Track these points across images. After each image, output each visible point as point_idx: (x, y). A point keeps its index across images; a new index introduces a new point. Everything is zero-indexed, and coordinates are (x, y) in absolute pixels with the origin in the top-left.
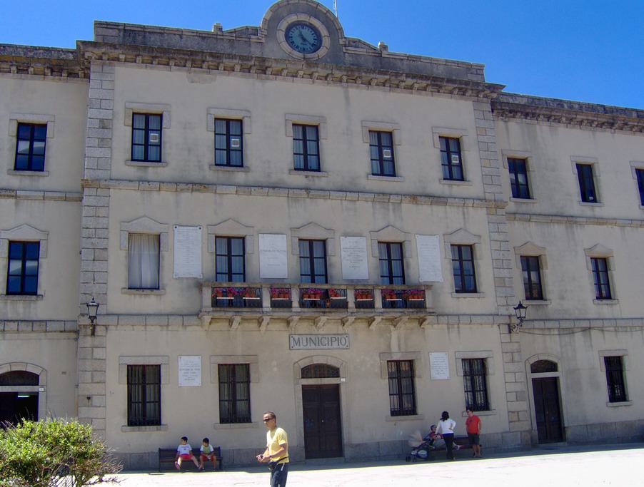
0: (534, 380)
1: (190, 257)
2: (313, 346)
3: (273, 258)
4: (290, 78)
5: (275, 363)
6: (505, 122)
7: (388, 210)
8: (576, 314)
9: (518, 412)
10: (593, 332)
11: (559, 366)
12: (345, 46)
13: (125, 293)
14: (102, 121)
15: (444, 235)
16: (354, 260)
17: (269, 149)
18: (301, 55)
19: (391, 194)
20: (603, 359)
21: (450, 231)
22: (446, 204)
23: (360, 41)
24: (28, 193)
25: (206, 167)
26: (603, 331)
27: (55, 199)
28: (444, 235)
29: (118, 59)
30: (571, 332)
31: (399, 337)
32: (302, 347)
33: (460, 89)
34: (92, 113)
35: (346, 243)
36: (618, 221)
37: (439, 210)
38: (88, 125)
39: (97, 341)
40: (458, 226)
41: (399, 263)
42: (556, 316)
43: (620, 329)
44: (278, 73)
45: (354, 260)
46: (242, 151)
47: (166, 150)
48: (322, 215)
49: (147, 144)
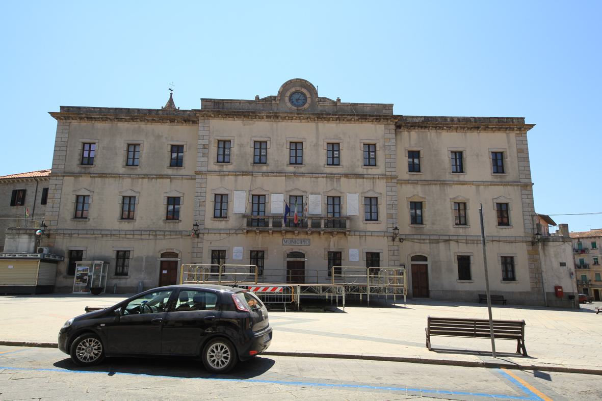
0: (412, 265)
1: (239, 204)
2: (293, 244)
3: (276, 205)
4: (290, 121)
6: (409, 132)
7: (334, 181)
10: (451, 242)
11: (428, 259)
12: (318, 102)
13: (212, 220)
14: (204, 145)
15: (361, 193)
16: (316, 206)
17: (278, 155)
18: (296, 108)
19: (335, 174)
20: (456, 257)
22: (363, 178)
23: (326, 98)
24: (175, 177)
25: (249, 164)
26: (458, 242)
27: (187, 179)
28: (361, 193)
29: (211, 117)
30: (437, 241)
31: (334, 243)
32: (288, 244)
34: (200, 142)
35: (311, 197)
36: (474, 183)
37: (360, 181)
38: (198, 147)
41: (338, 206)
42: (429, 233)
43: (469, 241)
44: (285, 118)
45: (316, 206)
46: (375, 158)
48: (302, 184)
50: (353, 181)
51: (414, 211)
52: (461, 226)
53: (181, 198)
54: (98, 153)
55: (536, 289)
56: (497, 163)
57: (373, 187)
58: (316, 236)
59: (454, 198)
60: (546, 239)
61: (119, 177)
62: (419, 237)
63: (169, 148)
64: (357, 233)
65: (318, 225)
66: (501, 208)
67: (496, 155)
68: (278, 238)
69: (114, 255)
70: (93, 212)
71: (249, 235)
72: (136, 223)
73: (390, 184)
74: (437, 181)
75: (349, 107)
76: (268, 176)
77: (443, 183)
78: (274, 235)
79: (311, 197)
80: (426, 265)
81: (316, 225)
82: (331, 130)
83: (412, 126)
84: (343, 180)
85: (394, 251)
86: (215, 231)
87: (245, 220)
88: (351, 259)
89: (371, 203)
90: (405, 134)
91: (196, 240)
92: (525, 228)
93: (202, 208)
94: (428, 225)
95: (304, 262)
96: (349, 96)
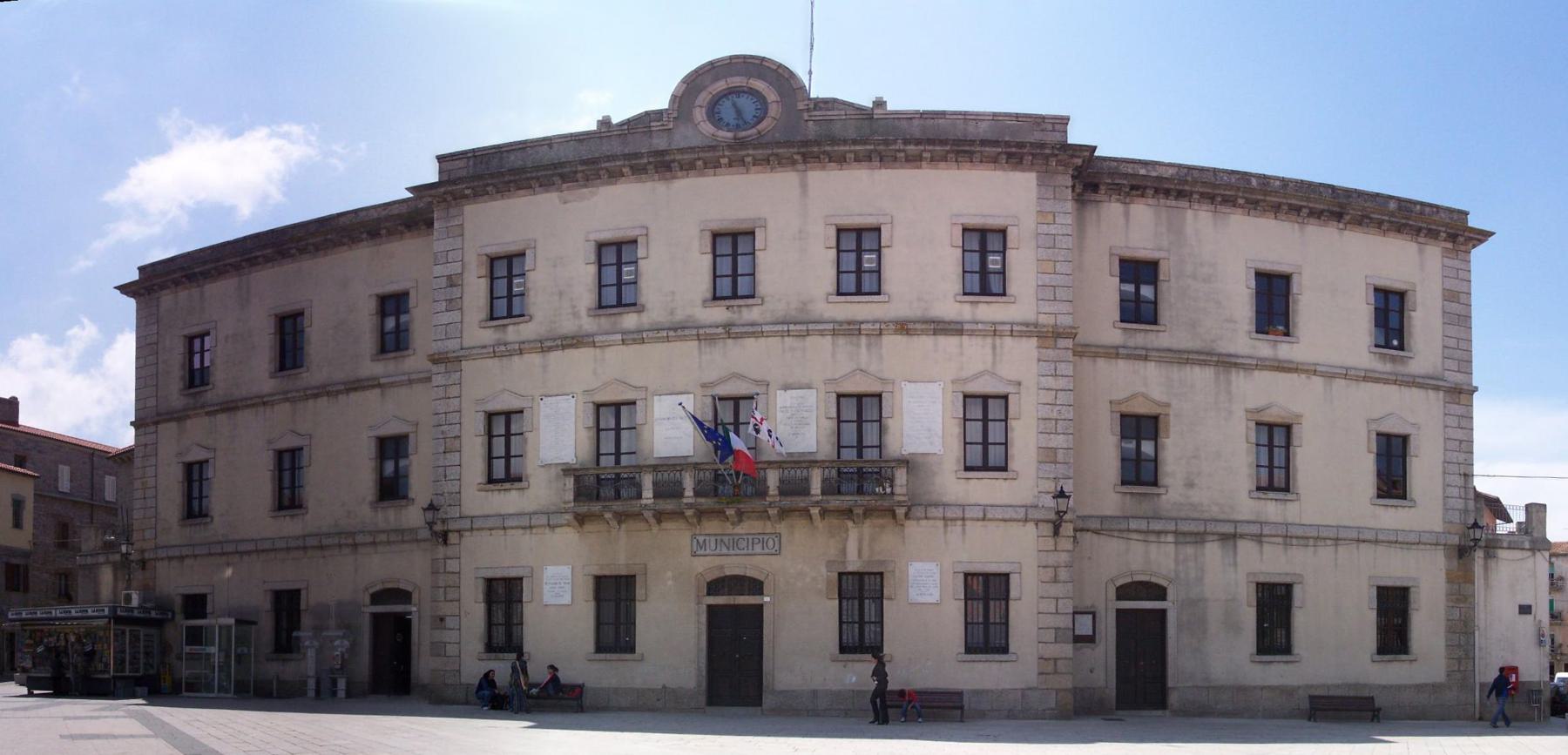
2: (725, 551)
5: (669, 574)
7: (858, 345)
8: (1215, 512)
9: (1056, 660)
12: (808, 110)
14: (449, 277)
16: (797, 424)
18: (730, 135)
21: (964, 374)
25: (583, 312)
26: (1261, 542)
30: (1199, 538)
31: (857, 546)
33: (1010, 155)
34: (439, 270)
35: (783, 399)
37: (949, 343)
39: (450, 551)
40: (981, 367)
42: (1174, 514)
45: (797, 424)
46: (1004, 273)
47: (887, 273)
49: (859, 271)
50: (926, 342)
51: (1132, 445)
52: (1271, 495)
53: (412, 436)
54: (217, 355)
55: (1459, 676)
56: (1387, 319)
57: (994, 363)
58: (800, 524)
59: (1259, 411)
60: (1492, 546)
61: (264, 404)
62: (1143, 525)
63: (371, 306)
64: (933, 512)
65: (803, 489)
66: (1389, 445)
67: (1387, 299)
68: (678, 536)
69: (265, 603)
70: (217, 501)
71: (588, 527)
72: (308, 517)
73: (1051, 353)
74: (1208, 354)
75: (916, 122)
76: (643, 341)
77: (1226, 363)
78: (664, 525)
79: (783, 399)
80: (1163, 612)
81: (794, 488)
82: (854, 191)
83: (1133, 188)
84: (892, 342)
85: (1056, 568)
86: (490, 523)
87: (570, 482)
88: (915, 595)
89: (984, 413)
90: (1112, 210)
91: (441, 551)
92: (1446, 510)
93: (453, 458)
94: (1173, 491)
95: (760, 607)
96: (911, 91)
